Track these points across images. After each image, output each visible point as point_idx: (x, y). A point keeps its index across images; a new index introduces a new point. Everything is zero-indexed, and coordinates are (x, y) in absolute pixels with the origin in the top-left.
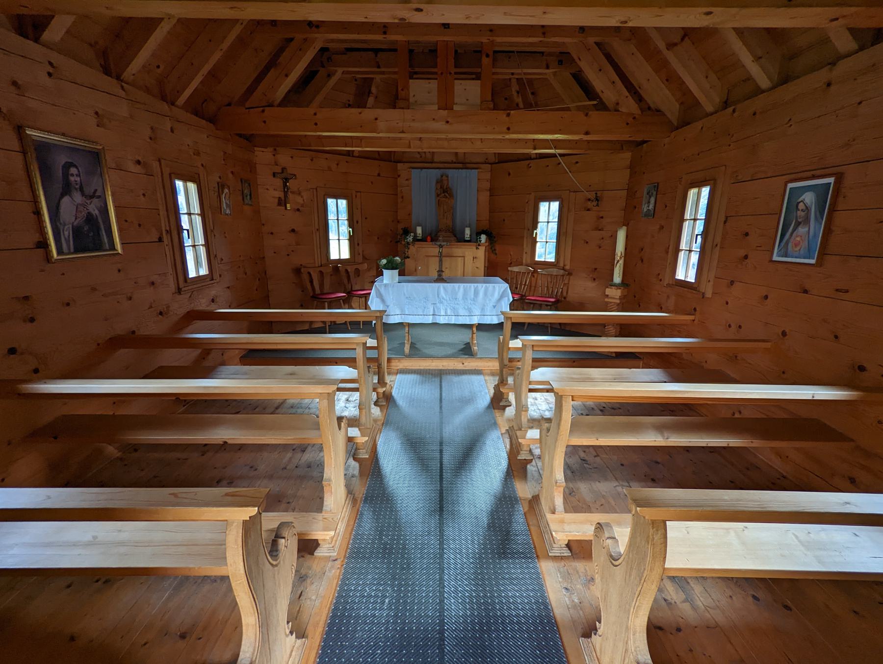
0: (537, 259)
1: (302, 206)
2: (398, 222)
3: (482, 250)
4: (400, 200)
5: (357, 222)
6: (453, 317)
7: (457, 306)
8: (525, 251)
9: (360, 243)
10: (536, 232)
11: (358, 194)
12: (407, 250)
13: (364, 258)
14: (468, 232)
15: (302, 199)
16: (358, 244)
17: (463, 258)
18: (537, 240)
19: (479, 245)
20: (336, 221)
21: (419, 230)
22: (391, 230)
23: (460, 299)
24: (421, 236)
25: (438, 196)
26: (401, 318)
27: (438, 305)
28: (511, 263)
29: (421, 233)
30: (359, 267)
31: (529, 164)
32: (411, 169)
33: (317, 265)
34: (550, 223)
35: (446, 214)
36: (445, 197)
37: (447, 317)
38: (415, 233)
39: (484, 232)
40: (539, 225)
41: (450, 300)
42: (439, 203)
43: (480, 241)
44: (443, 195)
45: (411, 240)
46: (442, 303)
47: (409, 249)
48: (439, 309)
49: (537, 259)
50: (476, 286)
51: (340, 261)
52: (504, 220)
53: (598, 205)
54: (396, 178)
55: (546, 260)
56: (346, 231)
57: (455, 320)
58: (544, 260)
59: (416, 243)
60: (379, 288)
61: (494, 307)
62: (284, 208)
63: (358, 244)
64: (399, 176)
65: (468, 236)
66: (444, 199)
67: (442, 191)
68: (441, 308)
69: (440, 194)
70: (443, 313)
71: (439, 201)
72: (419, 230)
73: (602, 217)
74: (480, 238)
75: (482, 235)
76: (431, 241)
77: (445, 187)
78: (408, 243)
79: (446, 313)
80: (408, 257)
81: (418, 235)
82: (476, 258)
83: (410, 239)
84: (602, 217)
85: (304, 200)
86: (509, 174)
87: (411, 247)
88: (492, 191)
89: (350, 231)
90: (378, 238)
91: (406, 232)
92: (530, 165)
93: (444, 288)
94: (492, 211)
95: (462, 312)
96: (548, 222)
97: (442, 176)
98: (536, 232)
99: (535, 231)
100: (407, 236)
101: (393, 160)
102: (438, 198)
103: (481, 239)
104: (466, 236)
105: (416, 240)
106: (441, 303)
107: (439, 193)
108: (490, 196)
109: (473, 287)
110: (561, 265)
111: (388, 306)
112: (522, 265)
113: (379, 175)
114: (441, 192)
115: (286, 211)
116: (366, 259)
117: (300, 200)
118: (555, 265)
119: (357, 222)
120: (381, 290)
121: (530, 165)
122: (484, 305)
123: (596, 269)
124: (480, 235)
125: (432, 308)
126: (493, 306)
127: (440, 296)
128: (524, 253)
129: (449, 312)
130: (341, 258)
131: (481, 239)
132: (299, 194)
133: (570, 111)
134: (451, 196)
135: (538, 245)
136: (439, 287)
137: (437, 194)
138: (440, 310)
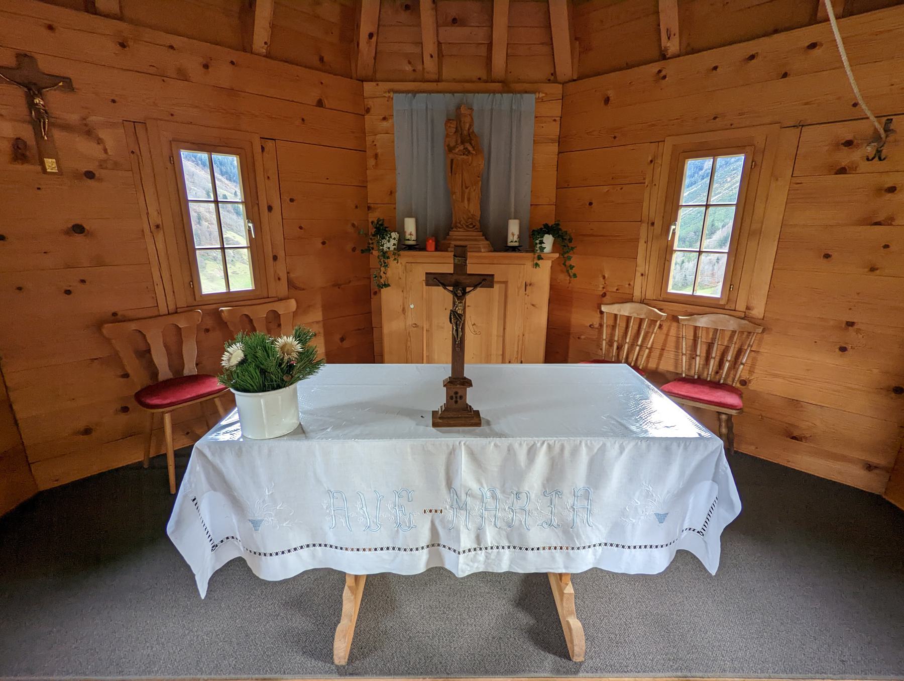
0: (670, 290)
1: (102, 165)
2: (369, 208)
3: (546, 266)
4: (371, 162)
5: (270, 208)
6: (507, 551)
7: (519, 517)
8: (640, 270)
9: (281, 254)
10: (674, 230)
11: (270, 145)
12: (383, 269)
13: (291, 284)
14: (514, 229)
15: (100, 147)
16: (275, 258)
17: (503, 285)
18: (675, 248)
19: (540, 258)
20: (213, 205)
21: (410, 226)
22: (353, 225)
23: (533, 496)
24: (414, 237)
25: (450, 149)
26: (314, 556)
27: (449, 514)
28: (604, 295)
29: (414, 232)
30: (280, 308)
31: (660, 71)
32: (391, 94)
33: (163, 310)
34: (711, 208)
35: (467, 191)
36: (467, 152)
37: (481, 555)
38: (402, 233)
39: (548, 230)
40: (682, 213)
41: (494, 497)
42: (452, 167)
43: (542, 249)
44: (461, 147)
45: (392, 248)
46: (460, 506)
47: (386, 266)
48: (454, 532)
49: (670, 290)
50: (597, 446)
51: (229, 298)
52: (591, 204)
53: (879, 155)
54: (364, 115)
55: (699, 293)
56: (243, 229)
57: (512, 561)
58: (690, 293)
59: (402, 253)
60: (216, 461)
61: (661, 518)
62: (39, 168)
63: (275, 258)
64: (368, 110)
65: (516, 238)
66: (465, 157)
67: (459, 141)
68: (462, 528)
69: (454, 147)
70: (466, 541)
71: (452, 160)
72: (410, 226)
73: (892, 190)
74: (541, 242)
75: (546, 235)
76: (436, 250)
77: (465, 132)
78: (385, 255)
79: (478, 539)
80: (388, 285)
81: (408, 237)
82: (530, 285)
83: (390, 244)
84: (892, 190)
85: (105, 151)
86: (607, 100)
87: (392, 263)
88: (563, 141)
89: (250, 227)
90: (324, 243)
91: (382, 230)
92: (663, 73)
93: (472, 455)
94: (562, 185)
95: (537, 535)
96: (707, 206)
97: (458, 108)
98: (674, 230)
99: (673, 227)
100: (384, 238)
101: (354, 76)
102: (451, 156)
103: (543, 245)
104: (510, 238)
105: (403, 246)
106: (460, 508)
107: (452, 144)
108: (559, 153)
109: (584, 450)
110: (741, 306)
111: (256, 524)
112: (631, 301)
113: (320, 103)
114: (456, 141)
115: (45, 176)
116: (296, 288)
117: (85, 147)
118: (723, 308)
119: (270, 208)
120: (224, 470)
121: (663, 73)
122: (623, 513)
123: (850, 324)
124: (542, 237)
125: (427, 526)
126: (657, 515)
127: (456, 485)
128: (638, 274)
129: (490, 537)
130: (232, 290)
131: (543, 245)
132: (89, 132)
133: (390, 286)
134: (478, 150)
135: (676, 258)
136: (452, 454)
137: (448, 146)
138: (458, 532)
